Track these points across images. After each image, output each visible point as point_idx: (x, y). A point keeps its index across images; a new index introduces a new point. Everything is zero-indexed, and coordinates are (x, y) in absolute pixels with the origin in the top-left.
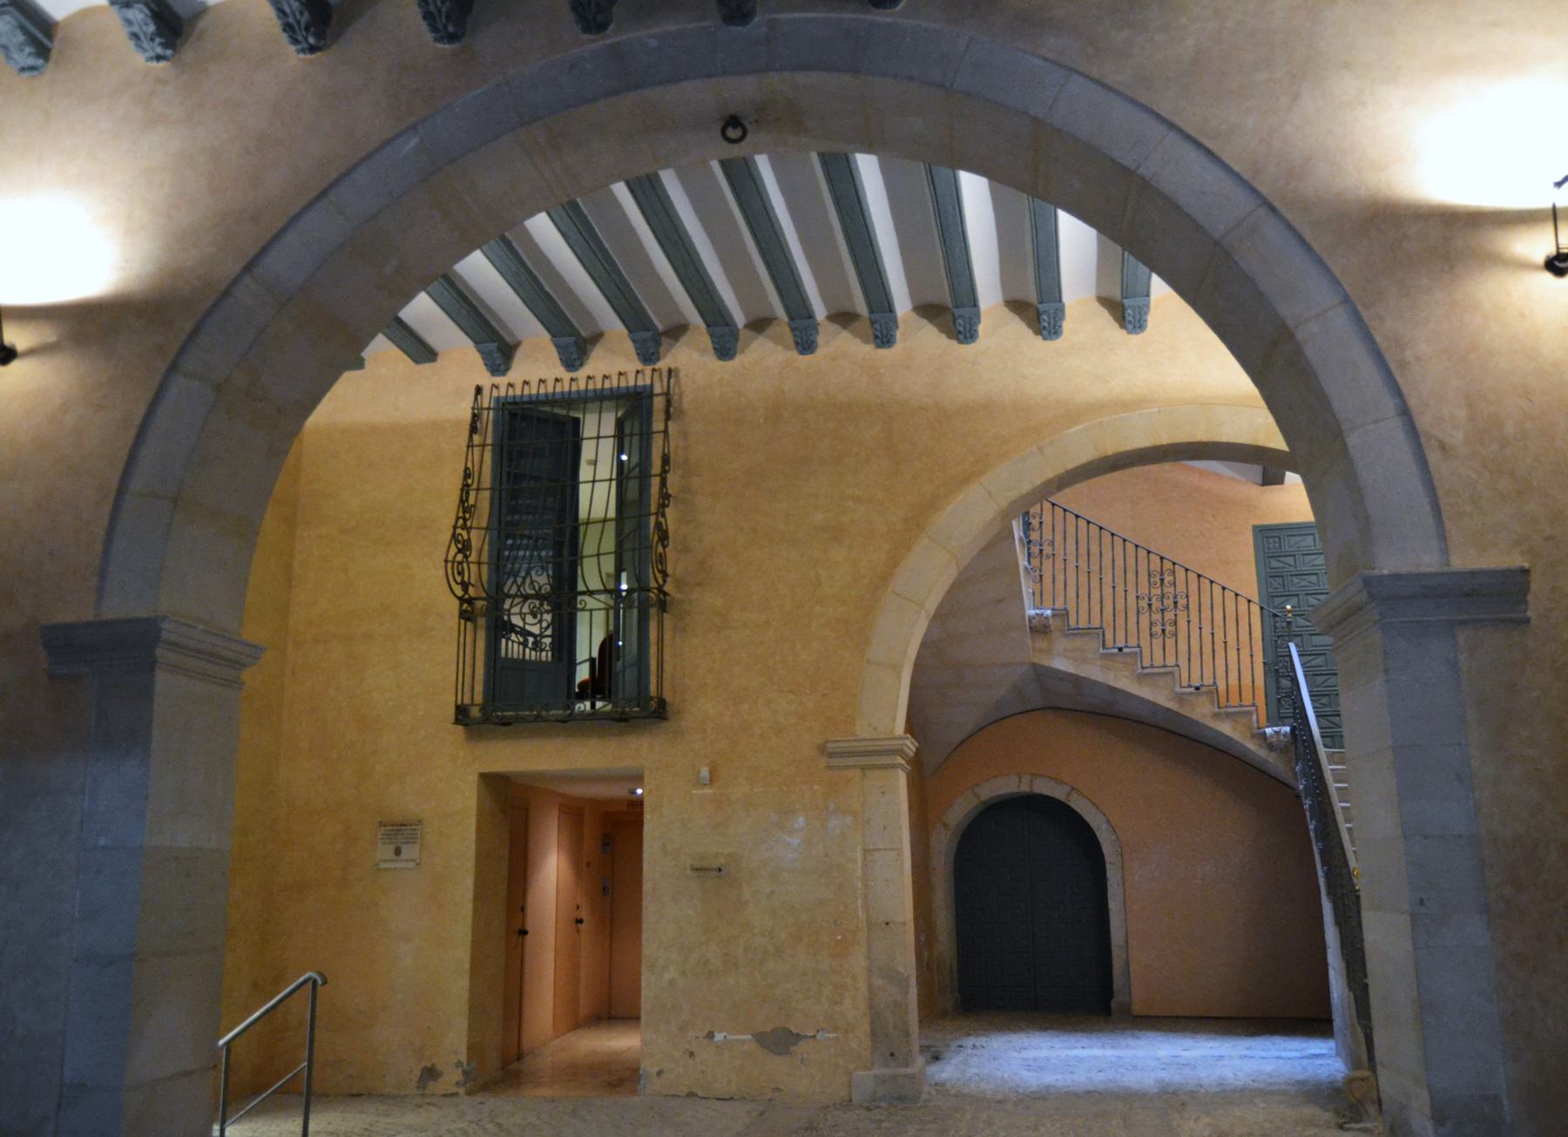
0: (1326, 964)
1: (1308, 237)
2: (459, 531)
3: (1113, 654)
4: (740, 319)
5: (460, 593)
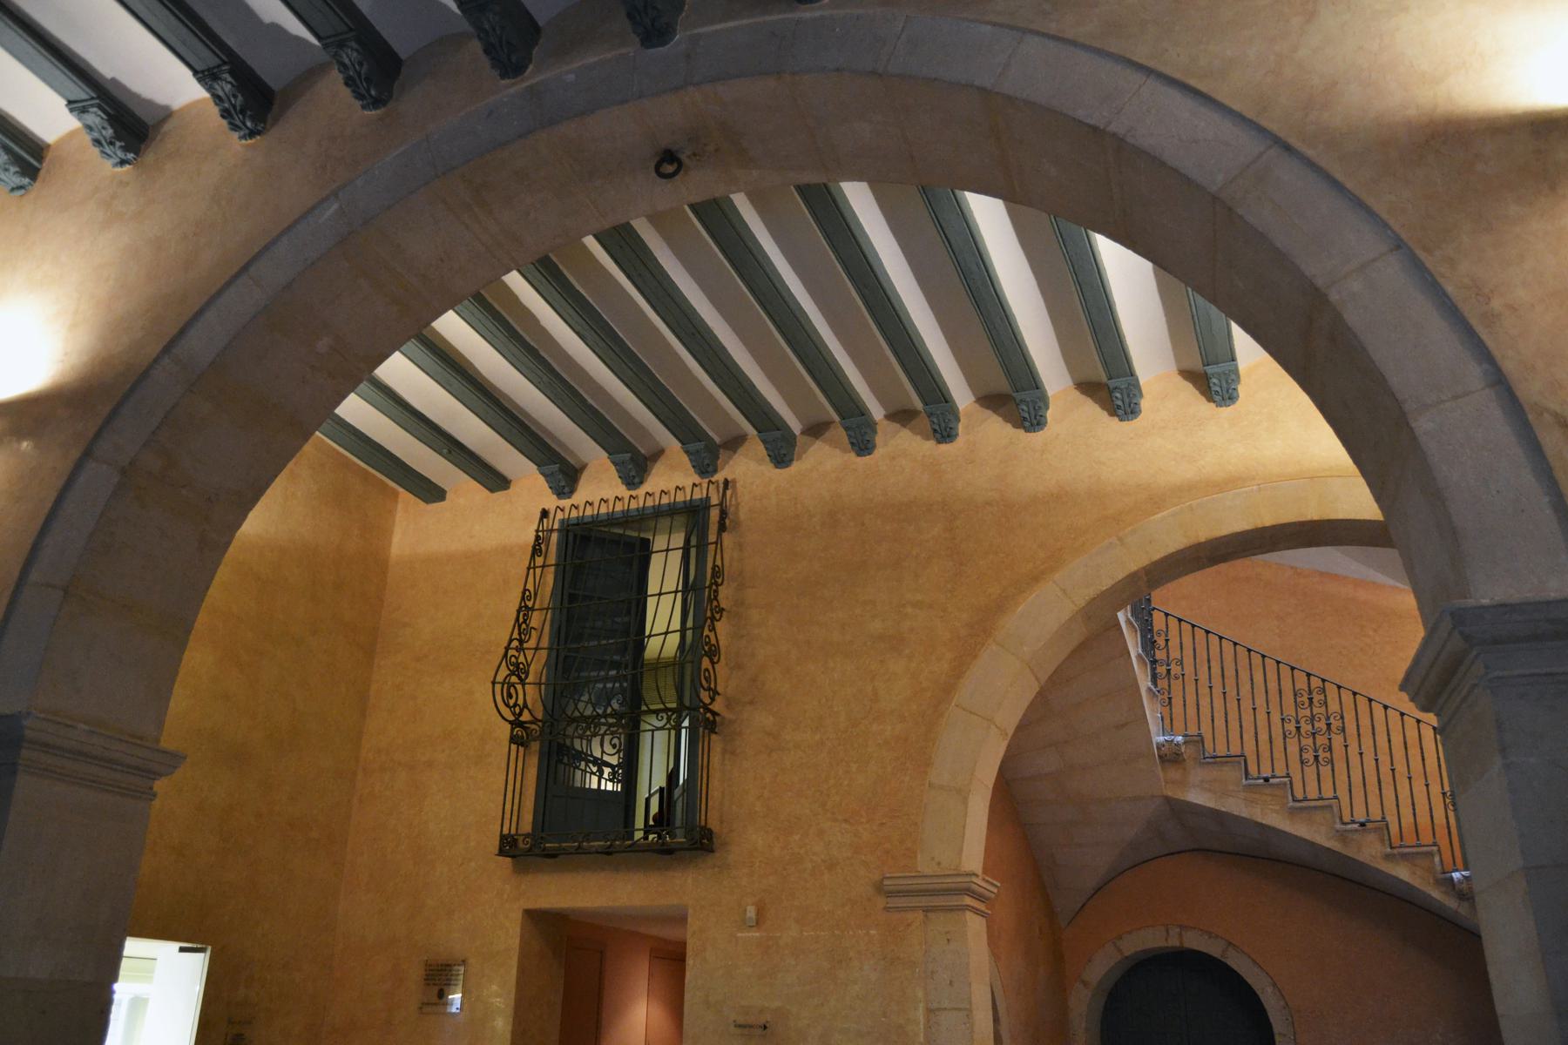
1: (1339, 176)
4: (795, 426)
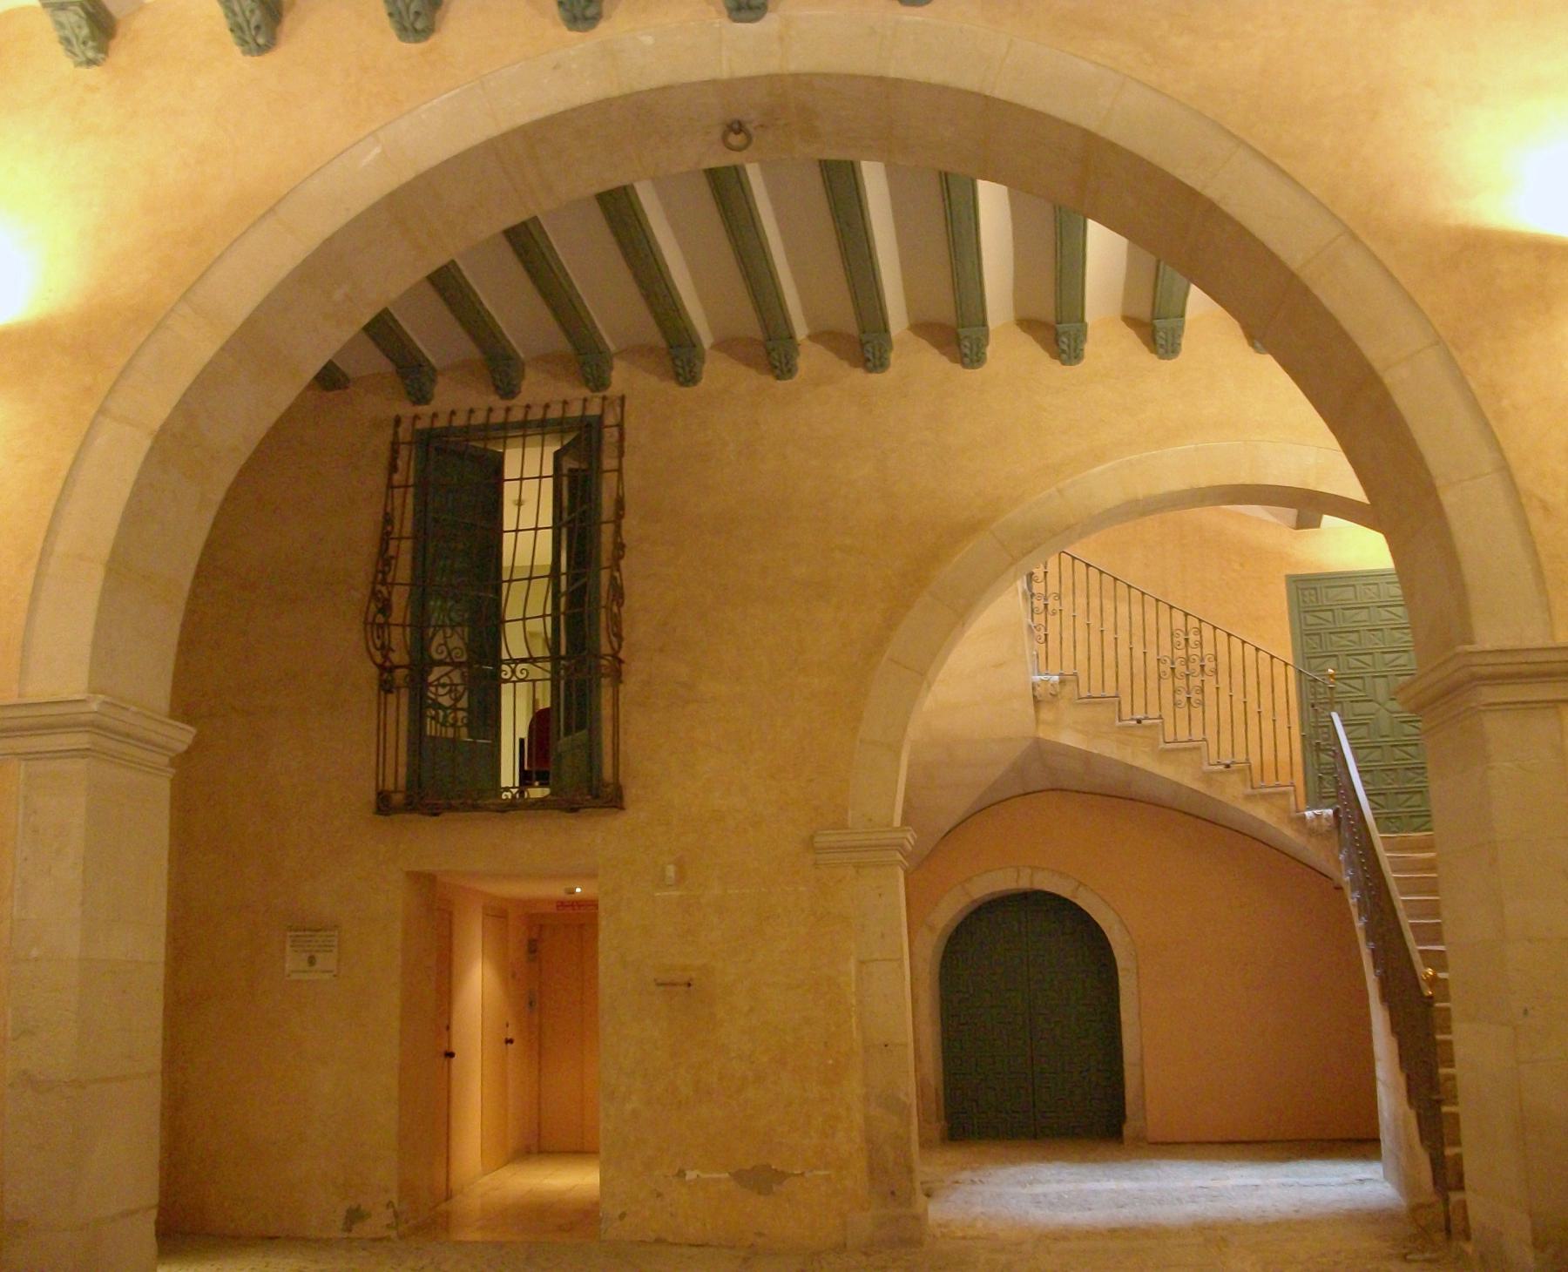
0: (1374, 1079)
2: (379, 587)
3: (1131, 727)
5: (379, 660)
